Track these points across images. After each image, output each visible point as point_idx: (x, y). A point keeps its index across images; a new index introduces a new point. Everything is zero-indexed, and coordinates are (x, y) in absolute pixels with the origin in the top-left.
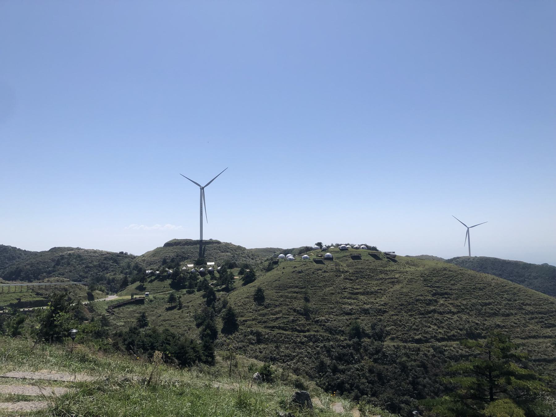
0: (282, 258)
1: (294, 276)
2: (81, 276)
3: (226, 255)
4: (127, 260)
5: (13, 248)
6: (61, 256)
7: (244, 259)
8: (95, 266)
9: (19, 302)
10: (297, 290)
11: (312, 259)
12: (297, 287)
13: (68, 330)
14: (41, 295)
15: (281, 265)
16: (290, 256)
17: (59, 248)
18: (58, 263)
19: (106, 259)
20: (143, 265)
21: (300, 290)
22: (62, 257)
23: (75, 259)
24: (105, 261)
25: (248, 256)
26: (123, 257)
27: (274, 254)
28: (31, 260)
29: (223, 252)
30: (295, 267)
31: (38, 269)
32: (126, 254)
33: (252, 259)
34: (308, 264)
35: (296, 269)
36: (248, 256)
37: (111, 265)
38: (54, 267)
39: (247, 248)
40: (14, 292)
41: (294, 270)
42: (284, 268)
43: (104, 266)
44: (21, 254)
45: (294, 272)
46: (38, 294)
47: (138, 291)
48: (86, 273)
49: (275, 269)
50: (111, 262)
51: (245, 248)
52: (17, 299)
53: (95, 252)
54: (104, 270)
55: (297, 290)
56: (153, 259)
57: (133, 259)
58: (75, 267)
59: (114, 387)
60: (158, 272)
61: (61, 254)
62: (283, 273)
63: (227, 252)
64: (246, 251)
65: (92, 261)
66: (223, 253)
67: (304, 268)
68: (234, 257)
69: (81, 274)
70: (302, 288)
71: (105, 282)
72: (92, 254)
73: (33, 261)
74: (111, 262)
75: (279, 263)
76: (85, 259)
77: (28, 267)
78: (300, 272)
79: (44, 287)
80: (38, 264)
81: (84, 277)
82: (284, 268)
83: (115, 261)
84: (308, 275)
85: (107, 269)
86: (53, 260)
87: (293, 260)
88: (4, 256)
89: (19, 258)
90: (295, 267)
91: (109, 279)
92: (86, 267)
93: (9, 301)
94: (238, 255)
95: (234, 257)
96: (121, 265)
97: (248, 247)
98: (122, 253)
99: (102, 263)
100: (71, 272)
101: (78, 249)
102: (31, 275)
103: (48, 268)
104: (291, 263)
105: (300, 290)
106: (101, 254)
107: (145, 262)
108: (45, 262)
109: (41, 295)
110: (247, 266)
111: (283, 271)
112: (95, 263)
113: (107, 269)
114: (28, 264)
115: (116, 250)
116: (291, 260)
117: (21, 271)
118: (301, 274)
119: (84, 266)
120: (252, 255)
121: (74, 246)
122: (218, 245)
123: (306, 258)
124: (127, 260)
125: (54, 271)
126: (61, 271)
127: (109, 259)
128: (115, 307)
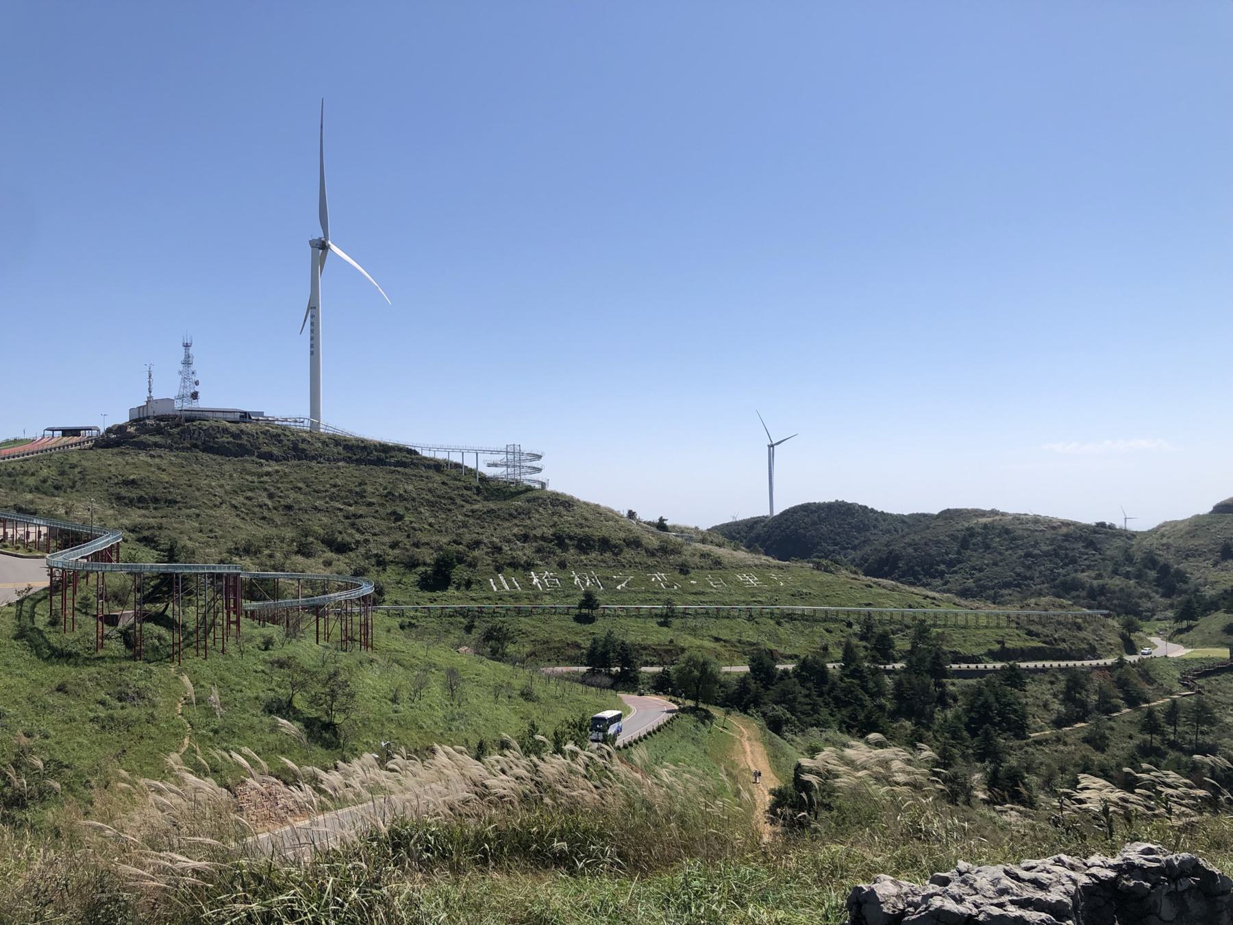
2: (1018, 575)
4: (1119, 542)
5: (861, 507)
6: (968, 529)
8: (1047, 554)
9: (1003, 647)
14: (1037, 635)
17: (957, 511)
18: (964, 544)
19: (1067, 537)
20: (1166, 557)
22: (971, 532)
23: (999, 535)
24: (1066, 544)
26: (1106, 533)
28: (911, 536)
31: (930, 555)
32: (1111, 527)
37: (1081, 553)
38: (959, 553)
40: (986, 627)
43: (1066, 555)
44: (876, 519)
46: (1030, 633)
47: (721, 539)
48: (1029, 568)
50: (1080, 545)
52: (999, 642)
53: (1036, 520)
54: (1066, 565)
56: (1192, 543)
57: (1129, 539)
58: (1000, 554)
59: (410, 488)
61: (966, 525)
65: (1036, 543)
69: (1018, 570)
71: (1084, 594)
72: (1031, 526)
73: (917, 538)
74: (1080, 546)
76: (1022, 538)
77: (910, 550)
80: (926, 544)
81: (1026, 578)
83: (1091, 544)
85: (1074, 561)
86: (954, 538)
88: (850, 524)
89: (875, 527)
91: (1091, 587)
92: (1028, 555)
93: (985, 644)
96: (1108, 552)
98: (1102, 525)
99: (1060, 547)
100: (995, 564)
101: (994, 513)
102: (916, 568)
103: (947, 554)
106: (1053, 526)
107: (1172, 550)
108: (938, 542)
109: (1037, 635)
112: (1045, 548)
113: (1074, 561)
114: (910, 545)
115: (1089, 518)
117: (898, 558)
119: (1021, 553)
124: (1119, 542)
125: (960, 562)
126: (976, 562)
127: (1076, 539)
128: (1199, 676)
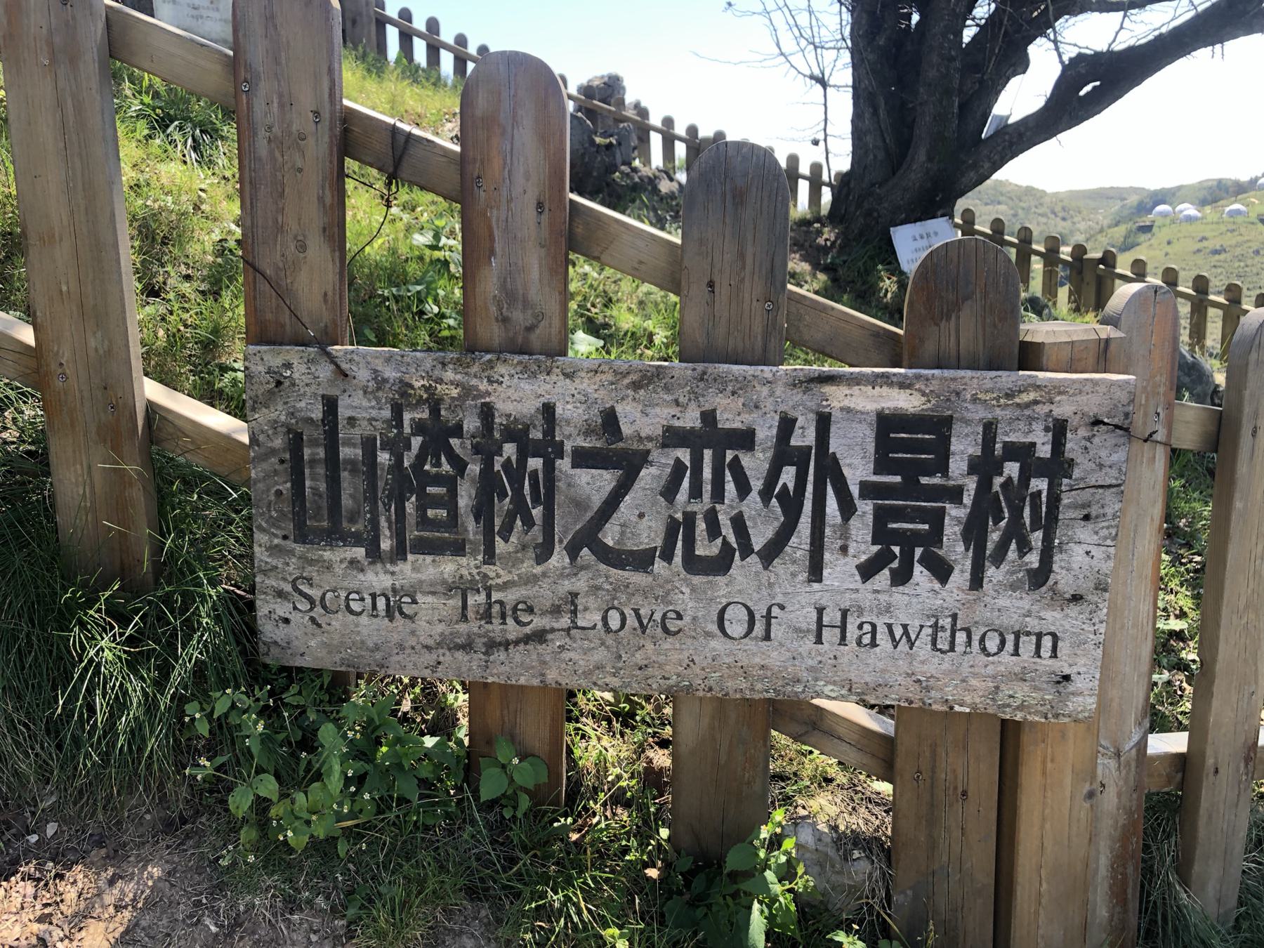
0: (1164, 215)
1: (1200, 262)
7: (1044, 220)
13: (63, 821)
15: (1161, 235)
16: (1189, 210)
27: (1120, 203)
29: (986, 204)
30: (1203, 239)
33: (1064, 219)
34: (1243, 230)
35: (1205, 243)
39: (1049, 190)
41: (1200, 245)
45: (1199, 251)
49: (1145, 245)
51: (1044, 191)
60: (653, 873)
62: (1167, 254)
63: (999, 203)
64: (1047, 200)
66: (990, 207)
67: (1229, 240)
68: (1015, 215)
75: (1154, 229)
78: (1216, 252)
82: (1169, 243)
84: (1241, 258)
87: (1196, 219)
90: (1203, 239)
94: (1027, 210)
95: (1015, 215)
97: (1050, 188)
116: (1190, 219)
118: (1222, 256)
120: (1064, 209)
123: (1238, 212)
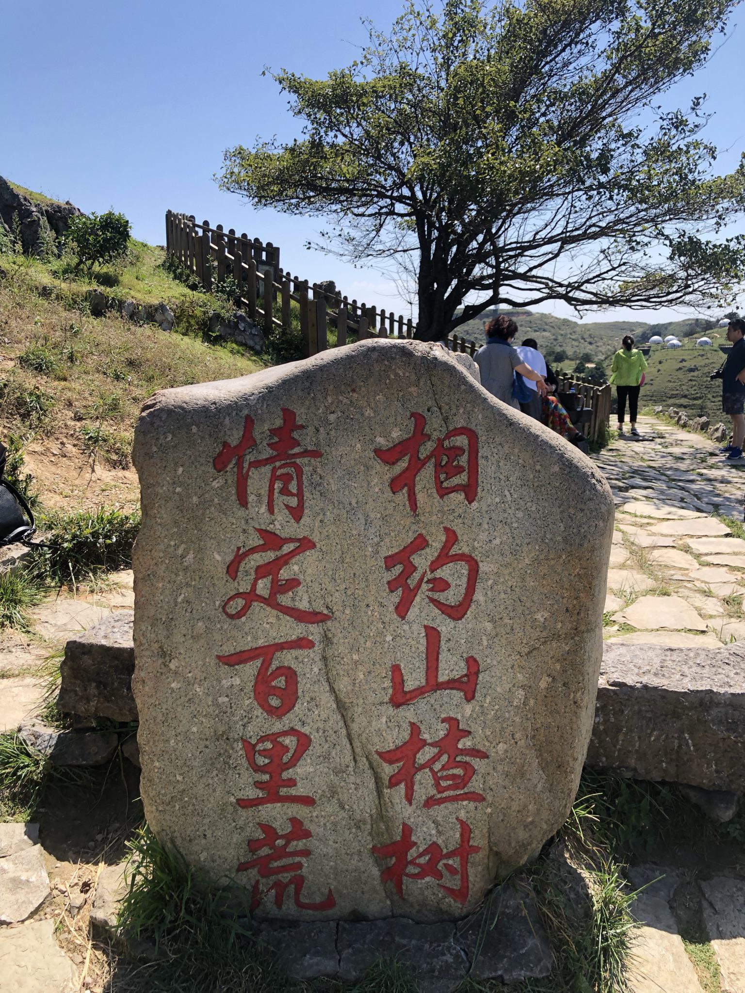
1: (681, 377)
3: (543, 337)
7: (576, 343)
10: (684, 401)
11: (716, 346)
12: (685, 396)
21: (691, 402)
25: (583, 338)
29: (535, 331)
30: (683, 360)
33: (590, 343)
35: (684, 364)
36: (583, 338)
41: (681, 365)
42: (660, 362)
45: (680, 369)
55: (684, 401)
62: (659, 371)
63: (545, 330)
64: (578, 329)
70: (695, 399)
75: (651, 353)
78: (691, 370)
79: (719, 478)
82: (660, 362)
87: (678, 346)
90: (683, 360)
95: (556, 340)
104: (675, 353)
105: (691, 402)
110: (587, 358)
111: (659, 367)
116: (674, 346)
118: (696, 373)
121: (621, 320)
122: (528, 318)
123: (706, 343)
